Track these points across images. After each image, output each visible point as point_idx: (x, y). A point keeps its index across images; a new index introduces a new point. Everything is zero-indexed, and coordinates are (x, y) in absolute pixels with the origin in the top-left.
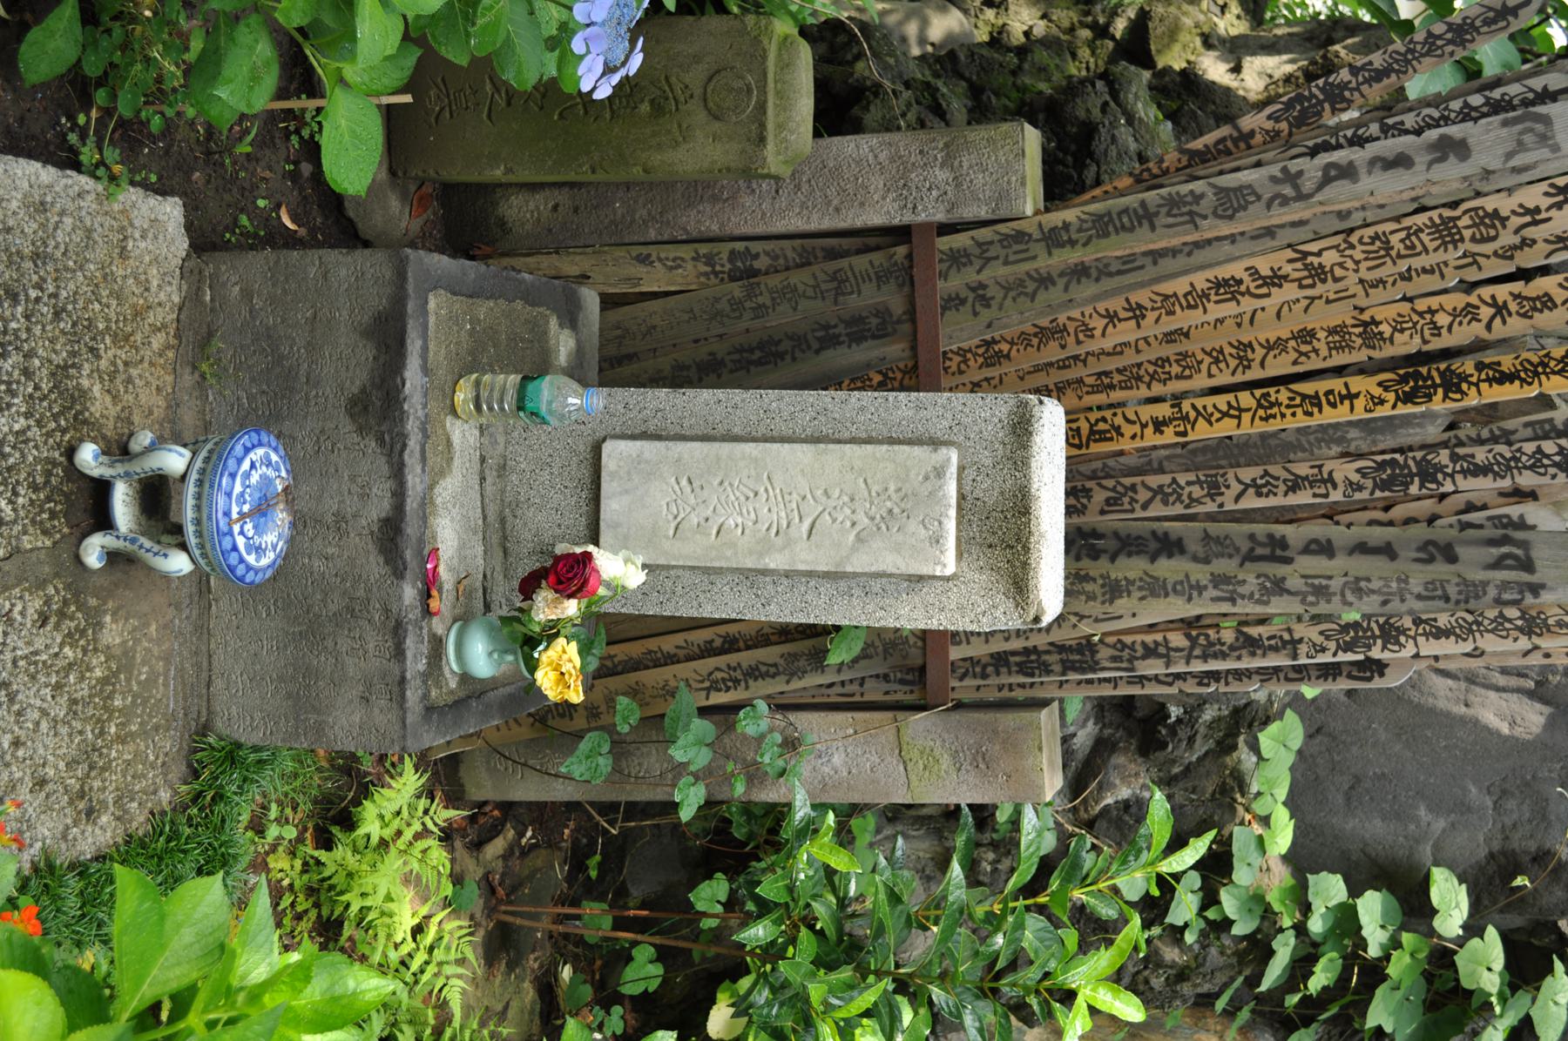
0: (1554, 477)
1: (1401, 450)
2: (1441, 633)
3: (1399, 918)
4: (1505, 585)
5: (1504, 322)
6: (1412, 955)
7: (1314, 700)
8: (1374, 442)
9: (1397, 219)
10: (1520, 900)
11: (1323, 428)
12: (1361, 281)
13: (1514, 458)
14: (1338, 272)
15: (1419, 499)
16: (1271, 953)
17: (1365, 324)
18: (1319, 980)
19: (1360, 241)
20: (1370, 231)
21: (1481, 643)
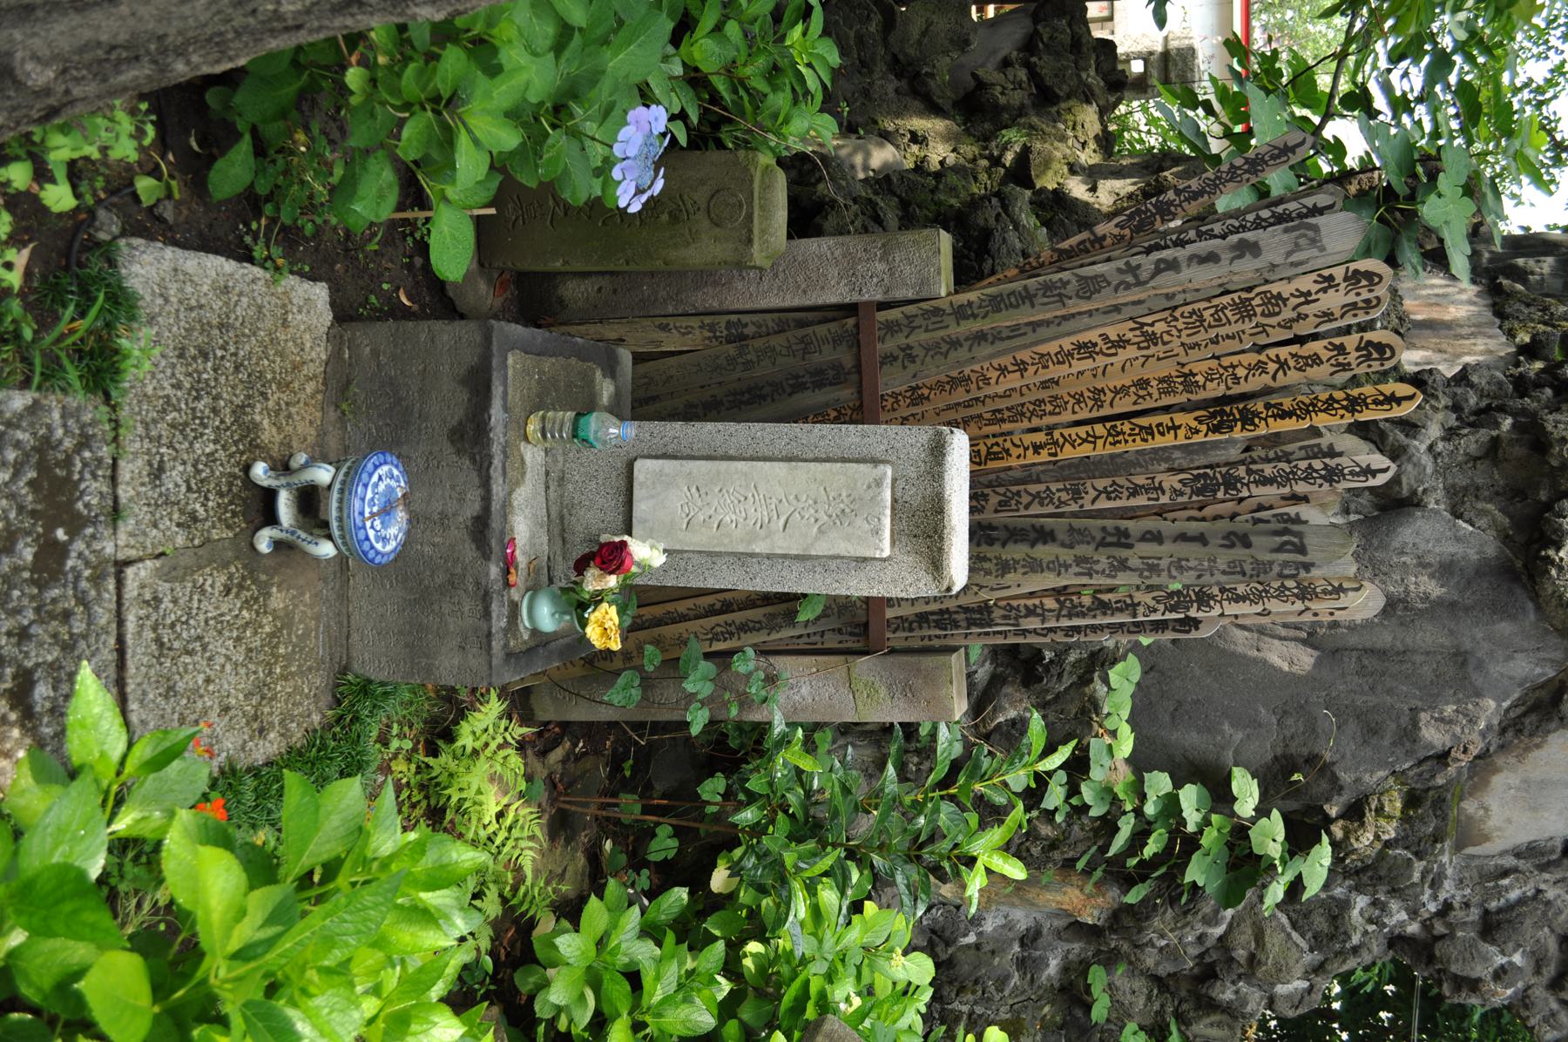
1: (1211, 467)
4: (1285, 564)
8: (1192, 461)
9: (1208, 300)
10: (1296, 791)
12: (1183, 344)
16: (1116, 830)
17: (1185, 376)
18: (1152, 848)
19: (1182, 315)
20: (1189, 308)
21: (1268, 606)
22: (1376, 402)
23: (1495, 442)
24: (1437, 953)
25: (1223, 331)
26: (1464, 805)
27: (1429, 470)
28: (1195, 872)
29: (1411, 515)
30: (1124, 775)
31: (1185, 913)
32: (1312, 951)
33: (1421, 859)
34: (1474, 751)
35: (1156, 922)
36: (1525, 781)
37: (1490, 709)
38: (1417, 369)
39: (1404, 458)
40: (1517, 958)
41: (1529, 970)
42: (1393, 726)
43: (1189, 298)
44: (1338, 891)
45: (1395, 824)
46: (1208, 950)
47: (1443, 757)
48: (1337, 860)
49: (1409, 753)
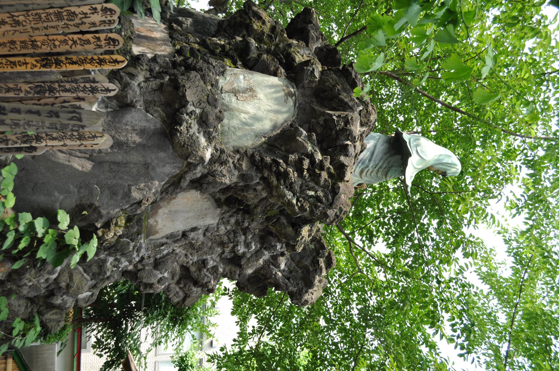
0: (89, 94)
1: (43, 82)
2: (54, 139)
3: (48, 225)
4: (74, 125)
5: (76, 46)
6: (52, 236)
7: (21, 159)
8: (35, 79)
9: (44, 9)
10: (85, 218)
11: (18, 73)
12: (32, 28)
13: (77, 88)
14: (24, 23)
15: (49, 98)
16: (6, 238)
17: (32, 41)
18: (23, 245)
19: (32, 15)
20: (35, 12)
21: (66, 142)
22: (110, 62)
23: (162, 84)
24: (139, 276)
25: (50, 24)
26: (149, 221)
27: (138, 93)
28: (41, 254)
29: (130, 110)
30: (11, 214)
31: (40, 271)
32: (91, 280)
33: (133, 242)
34: (151, 201)
35: (28, 276)
36: (170, 211)
37: (157, 185)
38: (138, 54)
39: (129, 88)
40: (166, 275)
41: (170, 278)
42: (122, 192)
43: (35, 7)
44: (102, 256)
45: (122, 229)
46: (50, 284)
47: (139, 203)
48: (100, 244)
49: (127, 202)
